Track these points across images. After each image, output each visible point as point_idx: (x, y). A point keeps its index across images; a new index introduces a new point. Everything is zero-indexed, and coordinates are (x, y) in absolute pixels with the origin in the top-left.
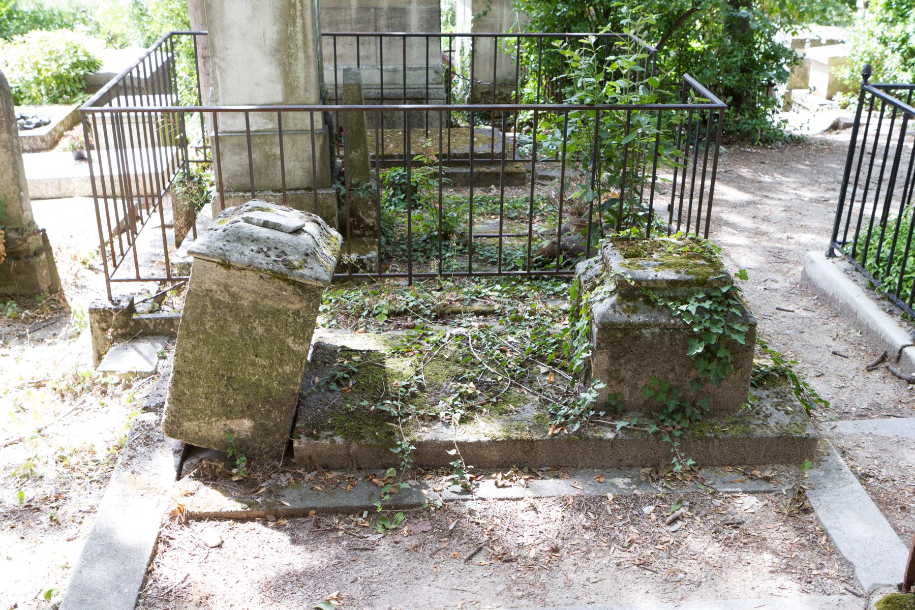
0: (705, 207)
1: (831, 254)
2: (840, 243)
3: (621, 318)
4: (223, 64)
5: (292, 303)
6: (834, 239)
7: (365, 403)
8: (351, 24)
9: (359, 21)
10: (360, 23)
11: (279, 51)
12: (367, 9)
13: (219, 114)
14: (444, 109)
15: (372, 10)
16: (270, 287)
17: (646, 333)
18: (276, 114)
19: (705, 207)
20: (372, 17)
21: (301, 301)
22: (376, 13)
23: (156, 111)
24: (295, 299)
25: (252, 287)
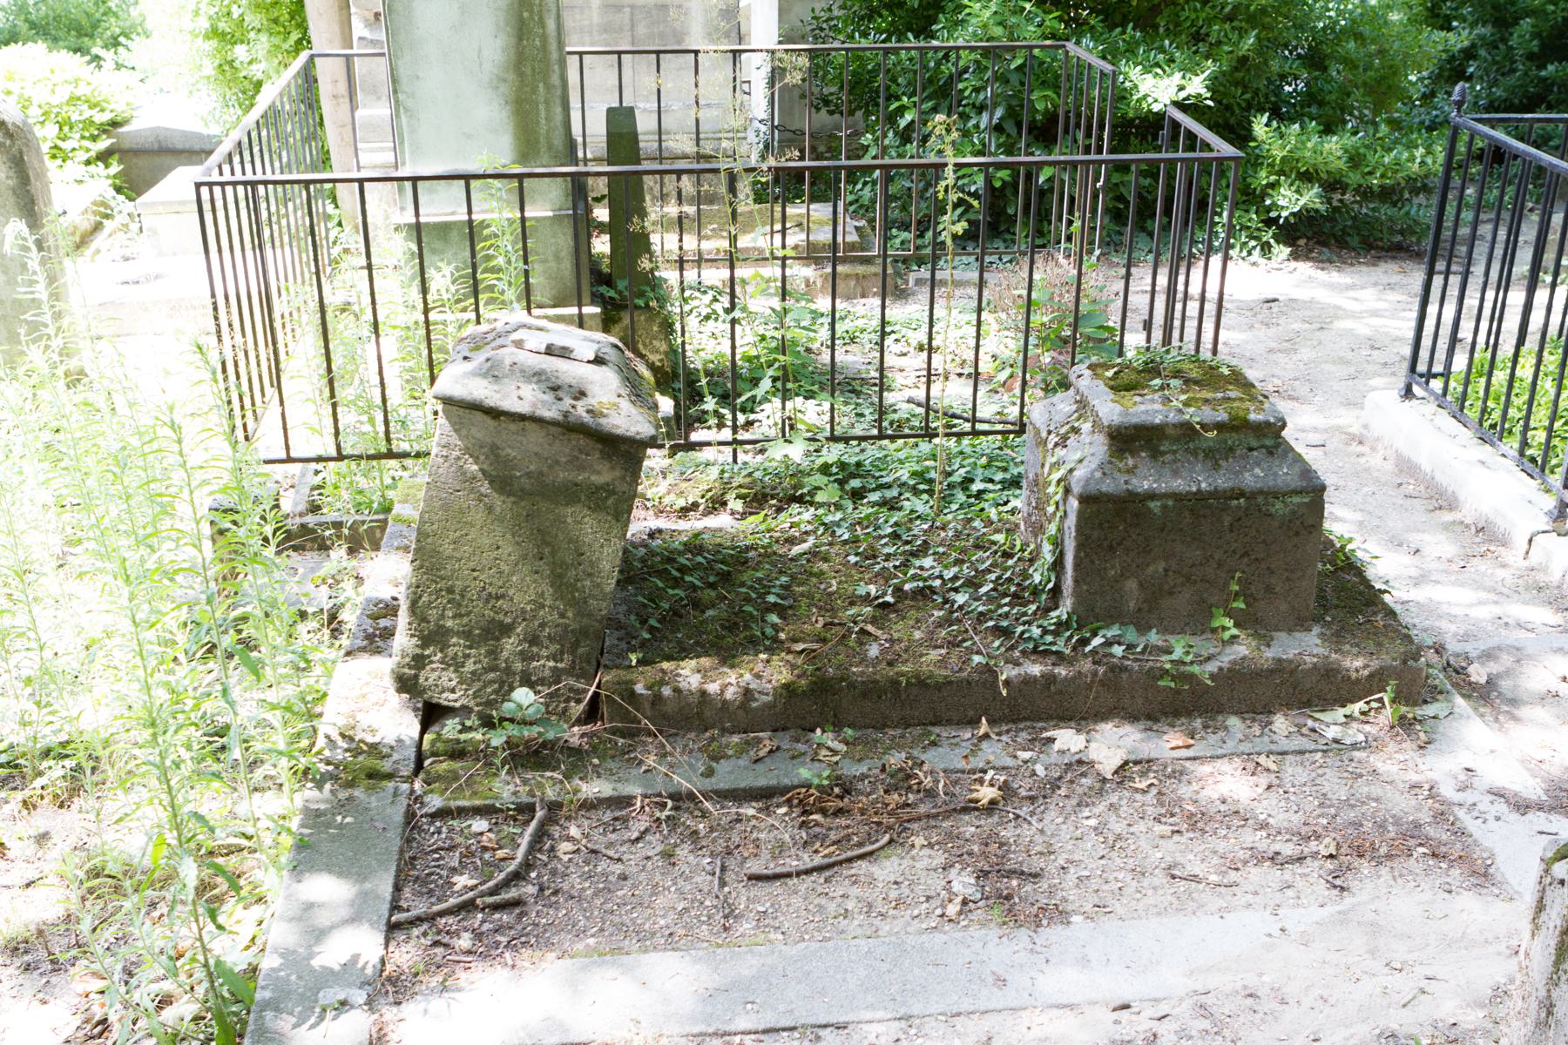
0: (1209, 327)
1: (1408, 393)
2: (1421, 376)
3: (1108, 486)
4: (410, 103)
5: (599, 473)
6: (1413, 369)
7: (348, 820)
8: (591, 33)
9: (606, 29)
10: (605, 31)
11: (505, 80)
12: (618, 8)
13: (366, 184)
14: (1082, 162)
15: (627, 10)
16: (562, 449)
17: (1154, 505)
18: (408, 185)
19: (1209, 327)
20: (627, 21)
21: (613, 468)
22: (632, 14)
23: (234, 184)
24: (604, 466)
25: (536, 449)
